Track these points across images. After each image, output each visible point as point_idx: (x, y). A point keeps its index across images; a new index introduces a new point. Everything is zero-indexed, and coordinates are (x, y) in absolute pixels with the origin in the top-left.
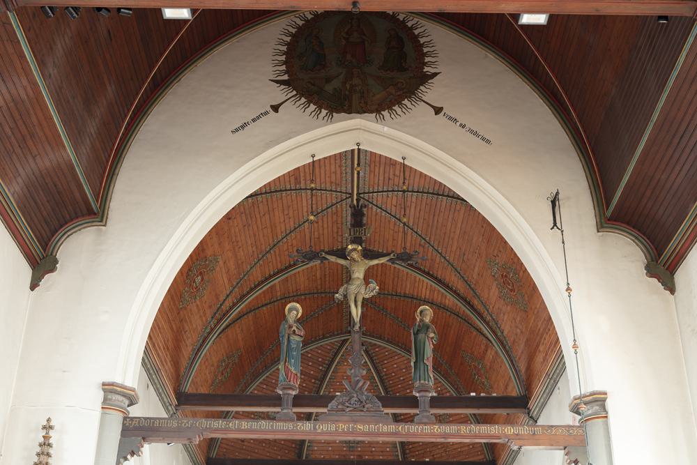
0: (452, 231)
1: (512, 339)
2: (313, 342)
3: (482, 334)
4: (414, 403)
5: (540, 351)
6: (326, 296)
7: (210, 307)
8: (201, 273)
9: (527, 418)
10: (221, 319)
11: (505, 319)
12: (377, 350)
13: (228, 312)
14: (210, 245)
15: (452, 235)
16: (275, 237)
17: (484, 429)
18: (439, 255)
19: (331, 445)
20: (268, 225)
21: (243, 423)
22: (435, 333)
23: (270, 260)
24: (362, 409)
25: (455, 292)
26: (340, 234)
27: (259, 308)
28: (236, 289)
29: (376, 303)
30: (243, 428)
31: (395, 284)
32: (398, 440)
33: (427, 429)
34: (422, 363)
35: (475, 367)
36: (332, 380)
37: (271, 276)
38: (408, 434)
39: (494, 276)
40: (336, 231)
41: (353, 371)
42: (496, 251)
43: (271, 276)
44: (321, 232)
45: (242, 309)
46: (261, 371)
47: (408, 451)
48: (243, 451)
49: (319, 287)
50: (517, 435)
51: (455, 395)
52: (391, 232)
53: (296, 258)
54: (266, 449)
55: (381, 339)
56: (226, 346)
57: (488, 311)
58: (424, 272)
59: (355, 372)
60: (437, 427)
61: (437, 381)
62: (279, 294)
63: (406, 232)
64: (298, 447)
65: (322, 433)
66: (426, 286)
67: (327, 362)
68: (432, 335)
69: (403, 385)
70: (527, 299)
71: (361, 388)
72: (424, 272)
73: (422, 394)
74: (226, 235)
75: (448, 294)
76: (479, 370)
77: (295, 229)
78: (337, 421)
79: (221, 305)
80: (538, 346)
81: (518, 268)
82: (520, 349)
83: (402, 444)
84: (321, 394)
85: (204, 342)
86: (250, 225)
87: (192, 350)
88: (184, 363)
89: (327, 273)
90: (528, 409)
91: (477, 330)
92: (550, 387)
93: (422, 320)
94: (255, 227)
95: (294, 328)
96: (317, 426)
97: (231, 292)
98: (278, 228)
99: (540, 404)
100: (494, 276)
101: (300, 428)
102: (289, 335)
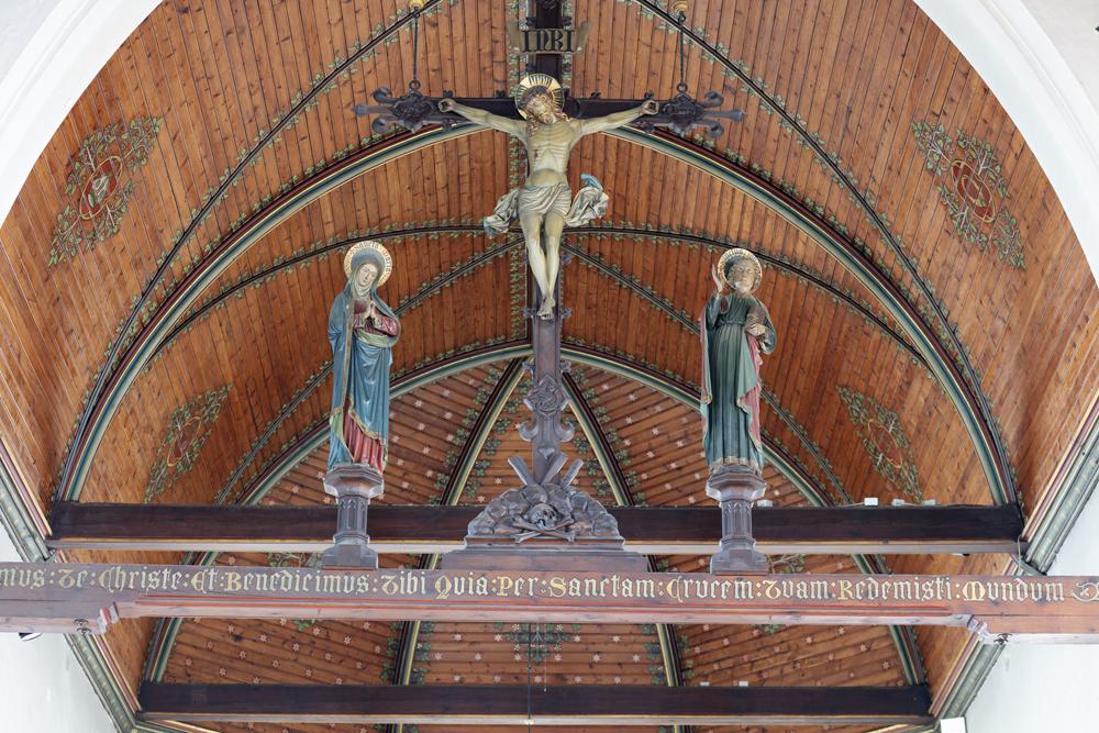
0: (817, 43)
1: (981, 349)
2: (427, 367)
3: (894, 334)
4: (706, 523)
5: (1058, 380)
6: (461, 237)
7: (137, 264)
8: (107, 168)
9: (1018, 567)
10: (169, 299)
11: (962, 293)
12: (606, 387)
13: (187, 279)
14: (130, 87)
15: (815, 57)
16: (315, 65)
17: (902, 587)
18: (778, 115)
19: (459, 628)
20: (296, 32)
21: (230, 575)
22: (766, 323)
23: (303, 132)
24: (563, 535)
25: (823, 221)
26: (499, 57)
27: (274, 269)
28: (209, 215)
29: (601, 254)
30: (230, 588)
31: (656, 197)
32: (661, 619)
33: (745, 588)
34: (731, 407)
35: (877, 431)
36: (480, 472)
37: (306, 180)
38: (693, 604)
39: (932, 172)
40: (486, 49)
41: (536, 431)
42: (939, 101)
43: (306, 180)
44: (446, 51)
45: (227, 272)
46: (285, 447)
47: (690, 663)
48: (236, 664)
49: (443, 211)
50: (996, 603)
51: (816, 505)
52: (645, 51)
53: (374, 116)
54: (303, 660)
55: (615, 357)
56: (186, 377)
57: (914, 271)
58: (736, 165)
59: (542, 432)
60: (772, 583)
61: (771, 473)
62: (330, 230)
63: (686, 49)
64: (389, 652)
65: (452, 603)
66: (739, 203)
67: (470, 412)
68: (759, 329)
69: (679, 483)
70: (1024, 233)
71: (558, 480)
72: (736, 165)
73: (729, 492)
74: (176, 57)
75: (802, 227)
76: (888, 438)
77: (373, 42)
78: (492, 569)
79: (168, 259)
80: (1053, 365)
81: (1002, 145)
82: (1002, 382)
83: (671, 629)
84: (455, 503)
85: (122, 361)
86: (243, 31)
87: (88, 387)
88: (68, 419)
89: (465, 170)
90: (1024, 540)
91: (884, 326)
92: (1084, 476)
93: (730, 289)
94: (258, 35)
95: (370, 312)
96: (438, 585)
97: (194, 223)
98: (325, 41)
99: (1056, 527)
100: (932, 172)
101: (390, 587)
102: (355, 330)
